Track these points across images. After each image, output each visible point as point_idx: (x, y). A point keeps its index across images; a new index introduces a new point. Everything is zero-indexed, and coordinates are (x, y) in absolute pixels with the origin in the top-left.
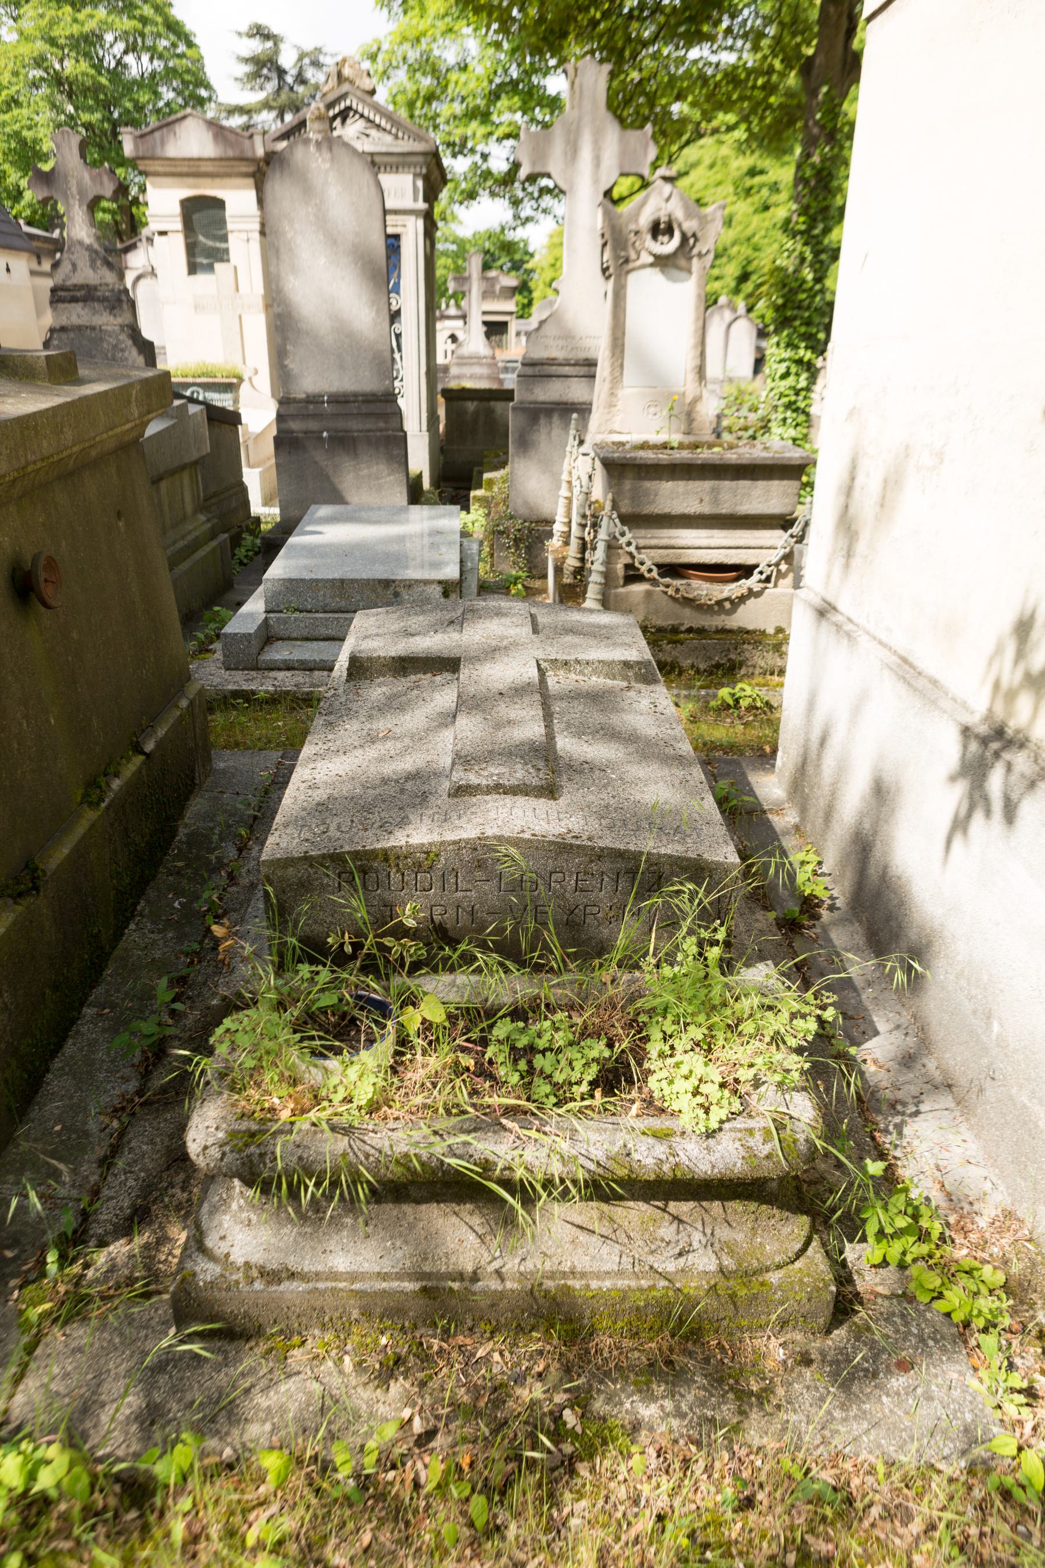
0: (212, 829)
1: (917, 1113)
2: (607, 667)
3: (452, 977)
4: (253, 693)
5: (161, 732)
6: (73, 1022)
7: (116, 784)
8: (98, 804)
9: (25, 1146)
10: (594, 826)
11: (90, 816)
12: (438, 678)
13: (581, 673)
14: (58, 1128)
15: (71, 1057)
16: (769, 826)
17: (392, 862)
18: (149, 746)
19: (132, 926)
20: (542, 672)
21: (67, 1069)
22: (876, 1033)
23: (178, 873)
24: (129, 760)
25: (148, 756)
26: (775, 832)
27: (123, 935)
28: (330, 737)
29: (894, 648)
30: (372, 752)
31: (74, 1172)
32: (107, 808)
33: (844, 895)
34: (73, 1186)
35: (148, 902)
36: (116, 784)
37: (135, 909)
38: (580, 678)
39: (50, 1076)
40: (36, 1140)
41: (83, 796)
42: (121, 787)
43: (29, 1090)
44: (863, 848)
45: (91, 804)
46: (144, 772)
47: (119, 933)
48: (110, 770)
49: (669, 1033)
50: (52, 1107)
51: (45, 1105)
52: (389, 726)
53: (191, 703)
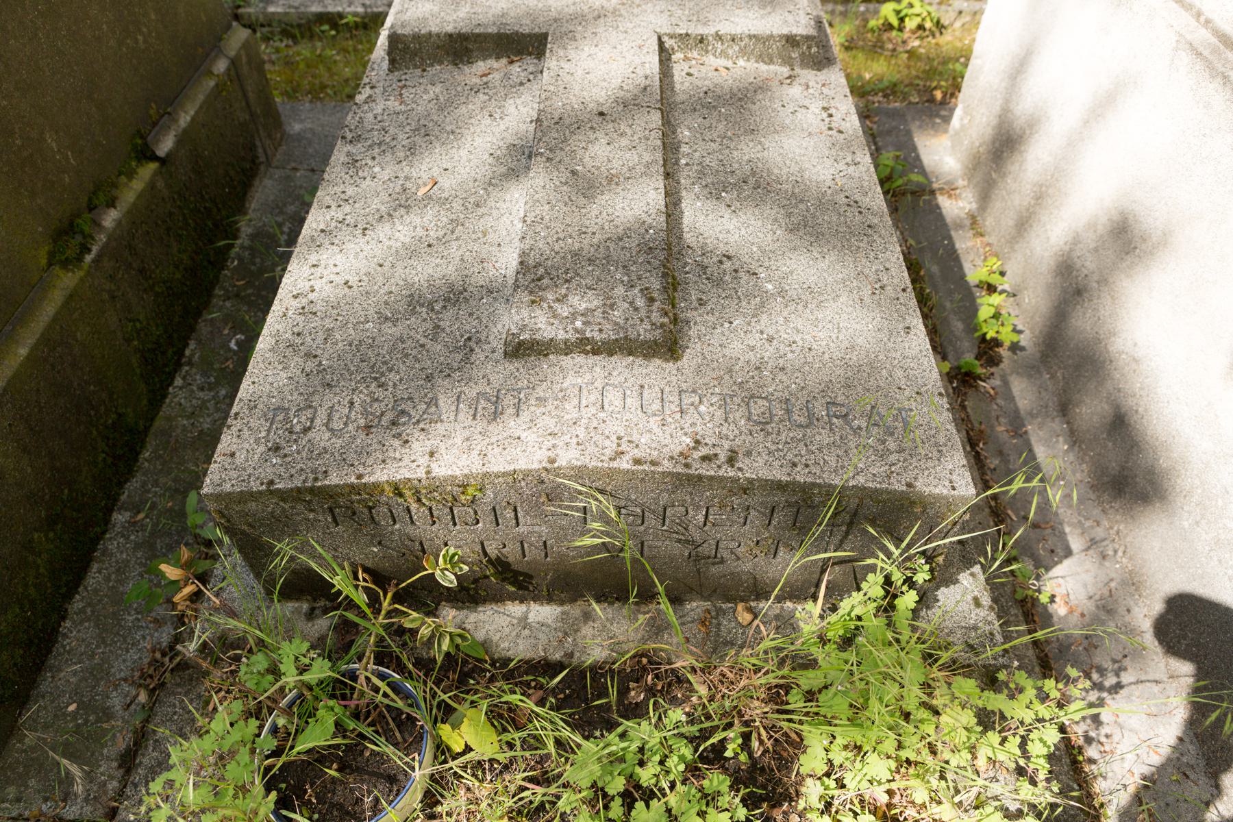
0: (280, 225)
1: (1118, 687)
2: (759, 46)
3: (523, 608)
4: (341, 16)
5: (184, 119)
6: (99, 538)
7: (110, 218)
8: (80, 259)
9: (30, 738)
10: (737, 431)
11: (67, 280)
12: (516, 68)
13: (724, 54)
14: (72, 708)
15: (96, 591)
16: (936, 210)
17: (408, 493)
18: (165, 145)
19: (178, 382)
20: (664, 53)
21: (89, 610)
22: (1068, 553)
23: (237, 295)
24: (131, 174)
25: (163, 161)
26: (946, 225)
27: (164, 396)
28: (350, 191)
29: (1208, 14)
30: (402, 232)
31: (89, 777)
32: (97, 261)
33: (1031, 329)
34: (86, 800)
35: (199, 342)
36: (110, 218)
37: (182, 354)
38: (722, 62)
39: (68, 623)
40: (46, 727)
41: (51, 255)
42: (119, 223)
43: (39, 646)
44: (1073, 287)
45: (65, 264)
46: (160, 184)
47: (158, 396)
48: (100, 195)
49: (836, 763)
50: (65, 674)
51: (60, 670)
52: (436, 172)
53: (234, 63)
